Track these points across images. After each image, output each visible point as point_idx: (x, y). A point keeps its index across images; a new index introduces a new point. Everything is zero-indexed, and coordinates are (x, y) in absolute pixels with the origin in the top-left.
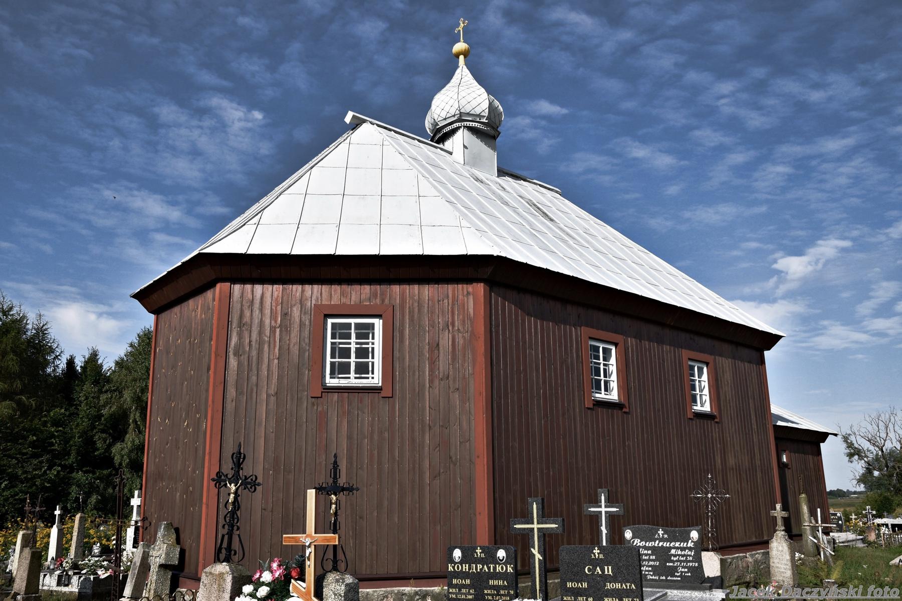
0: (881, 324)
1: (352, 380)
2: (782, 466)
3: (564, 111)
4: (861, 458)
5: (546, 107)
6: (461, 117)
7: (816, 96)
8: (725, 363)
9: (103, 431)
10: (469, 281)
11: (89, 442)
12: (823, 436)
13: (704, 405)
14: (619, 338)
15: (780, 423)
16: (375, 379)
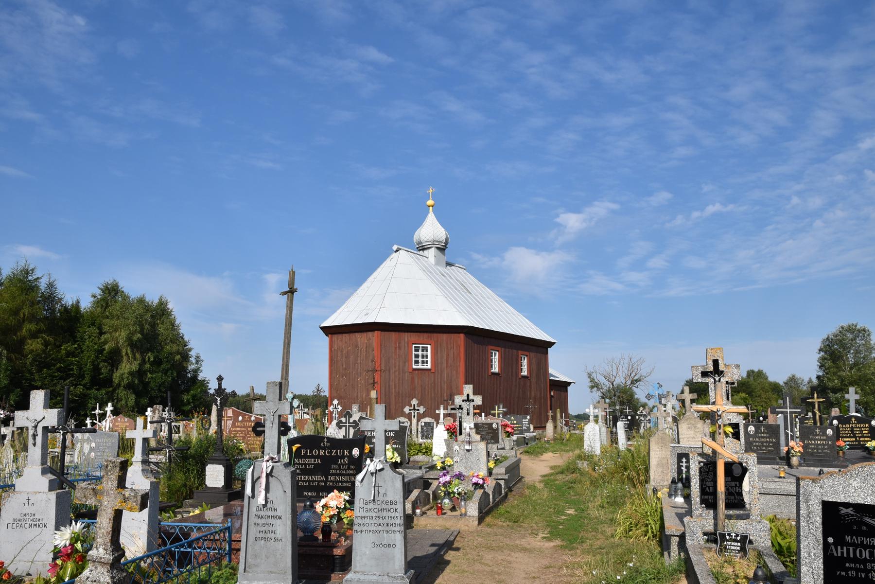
0: (635, 277)
1: (420, 366)
2: (551, 397)
3: (391, 60)
4: (598, 389)
5: (373, 54)
6: (434, 242)
7: (608, 77)
8: (533, 355)
9: (105, 361)
10: (459, 333)
11: (96, 369)
12: (569, 384)
13: (525, 373)
14: (499, 349)
15: (552, 378)
16: (429, 366)
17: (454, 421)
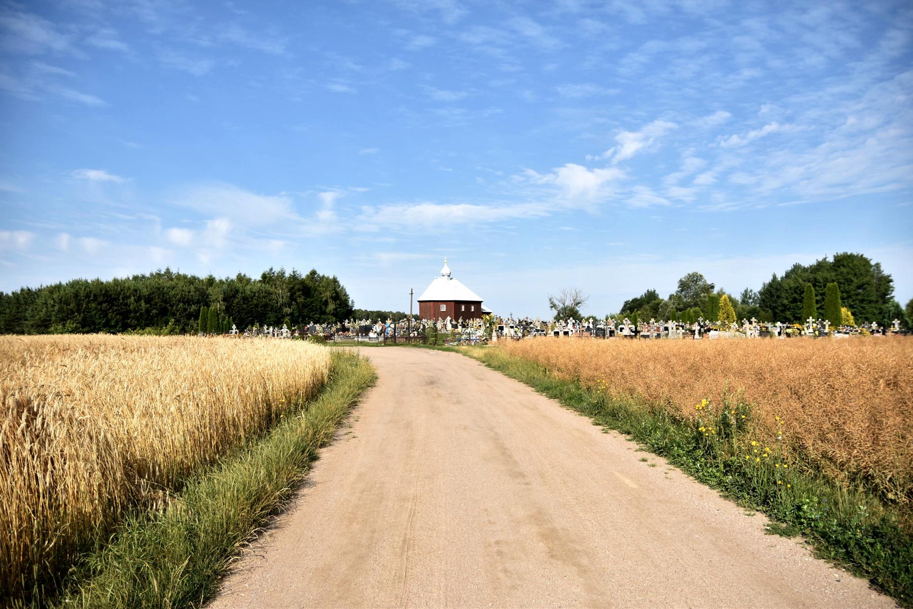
11: (321, 308)
17: (855, 377)
